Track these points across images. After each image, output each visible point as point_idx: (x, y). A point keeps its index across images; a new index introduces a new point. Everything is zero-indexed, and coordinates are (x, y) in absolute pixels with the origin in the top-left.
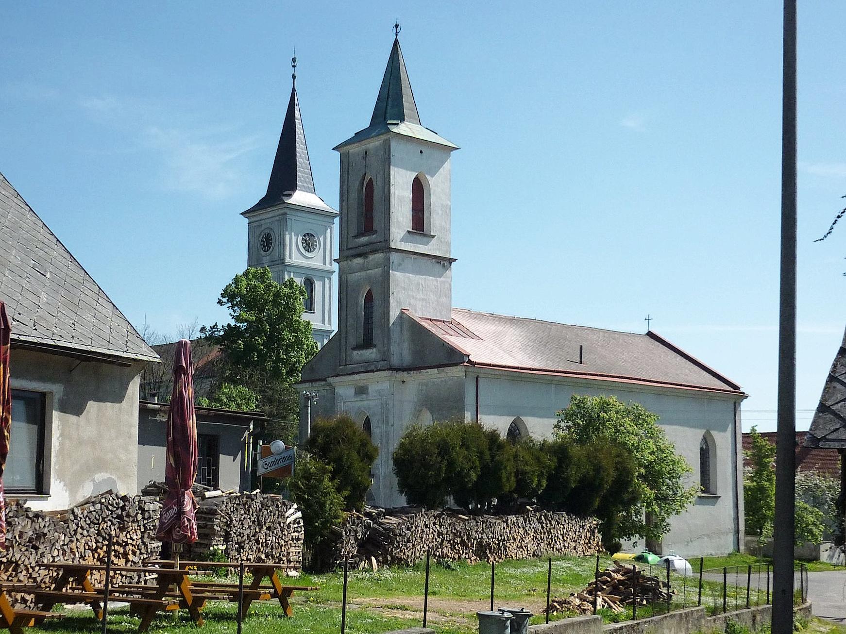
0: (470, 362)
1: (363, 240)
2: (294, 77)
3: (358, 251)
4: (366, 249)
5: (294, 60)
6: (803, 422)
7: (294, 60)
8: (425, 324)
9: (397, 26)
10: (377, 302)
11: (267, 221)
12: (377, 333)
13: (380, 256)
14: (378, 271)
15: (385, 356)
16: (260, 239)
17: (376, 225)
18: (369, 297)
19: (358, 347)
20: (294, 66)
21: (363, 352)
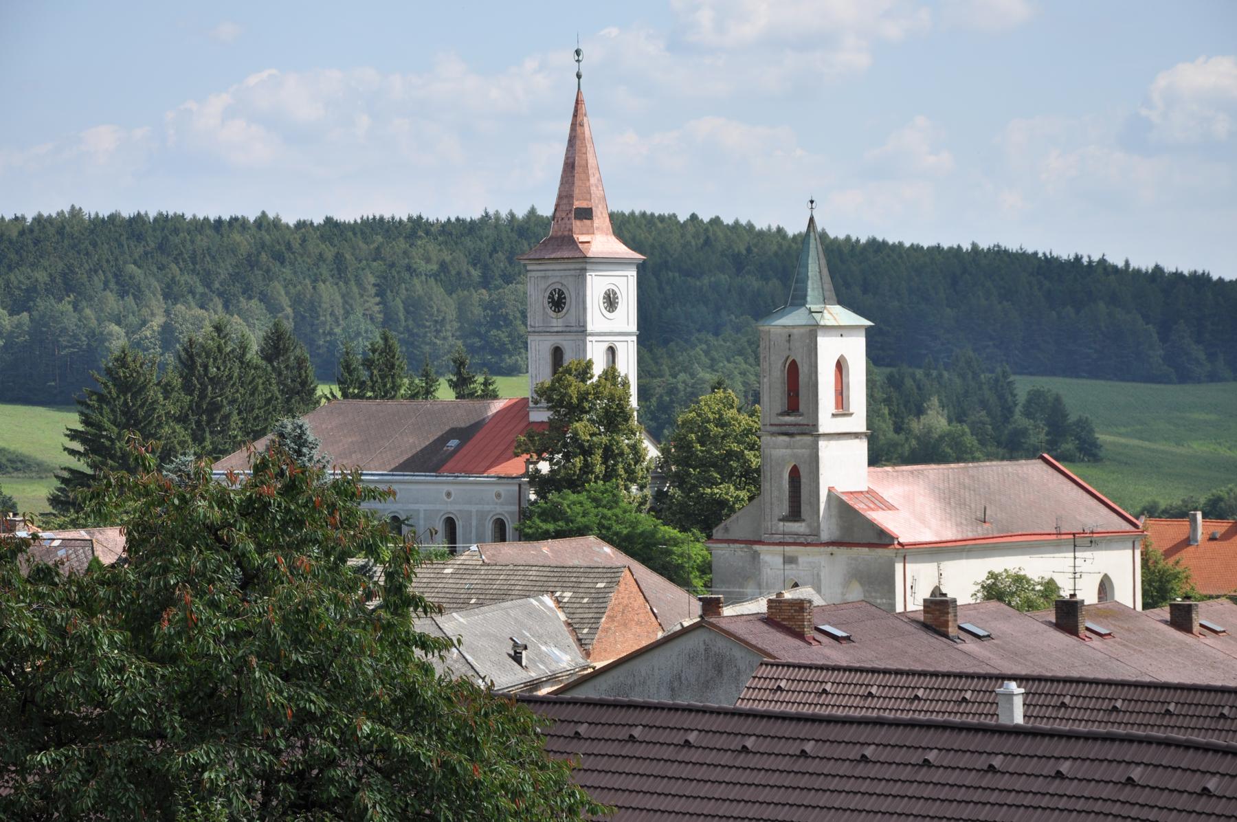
0: (899, 544)
1: (788, 419)
2: (579, 76)
3: (784, 429)
4: (793, 430)
5: (578, 52)
6: (365, 506)
7: (578, 52)
8: (844, 498)
9: (812, 202)
10: (804, 480)
11: (557, 273)
12: (805, 508)
13: (808, 439)
14: (806, 452)
15: (816, 533)
16: (547, 294)
17: (802, 407)
18: (795, 474)
19: (783, 519)
20: (578, 61)
21: (788, 524)
